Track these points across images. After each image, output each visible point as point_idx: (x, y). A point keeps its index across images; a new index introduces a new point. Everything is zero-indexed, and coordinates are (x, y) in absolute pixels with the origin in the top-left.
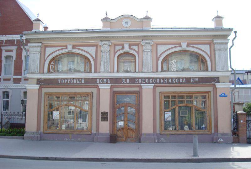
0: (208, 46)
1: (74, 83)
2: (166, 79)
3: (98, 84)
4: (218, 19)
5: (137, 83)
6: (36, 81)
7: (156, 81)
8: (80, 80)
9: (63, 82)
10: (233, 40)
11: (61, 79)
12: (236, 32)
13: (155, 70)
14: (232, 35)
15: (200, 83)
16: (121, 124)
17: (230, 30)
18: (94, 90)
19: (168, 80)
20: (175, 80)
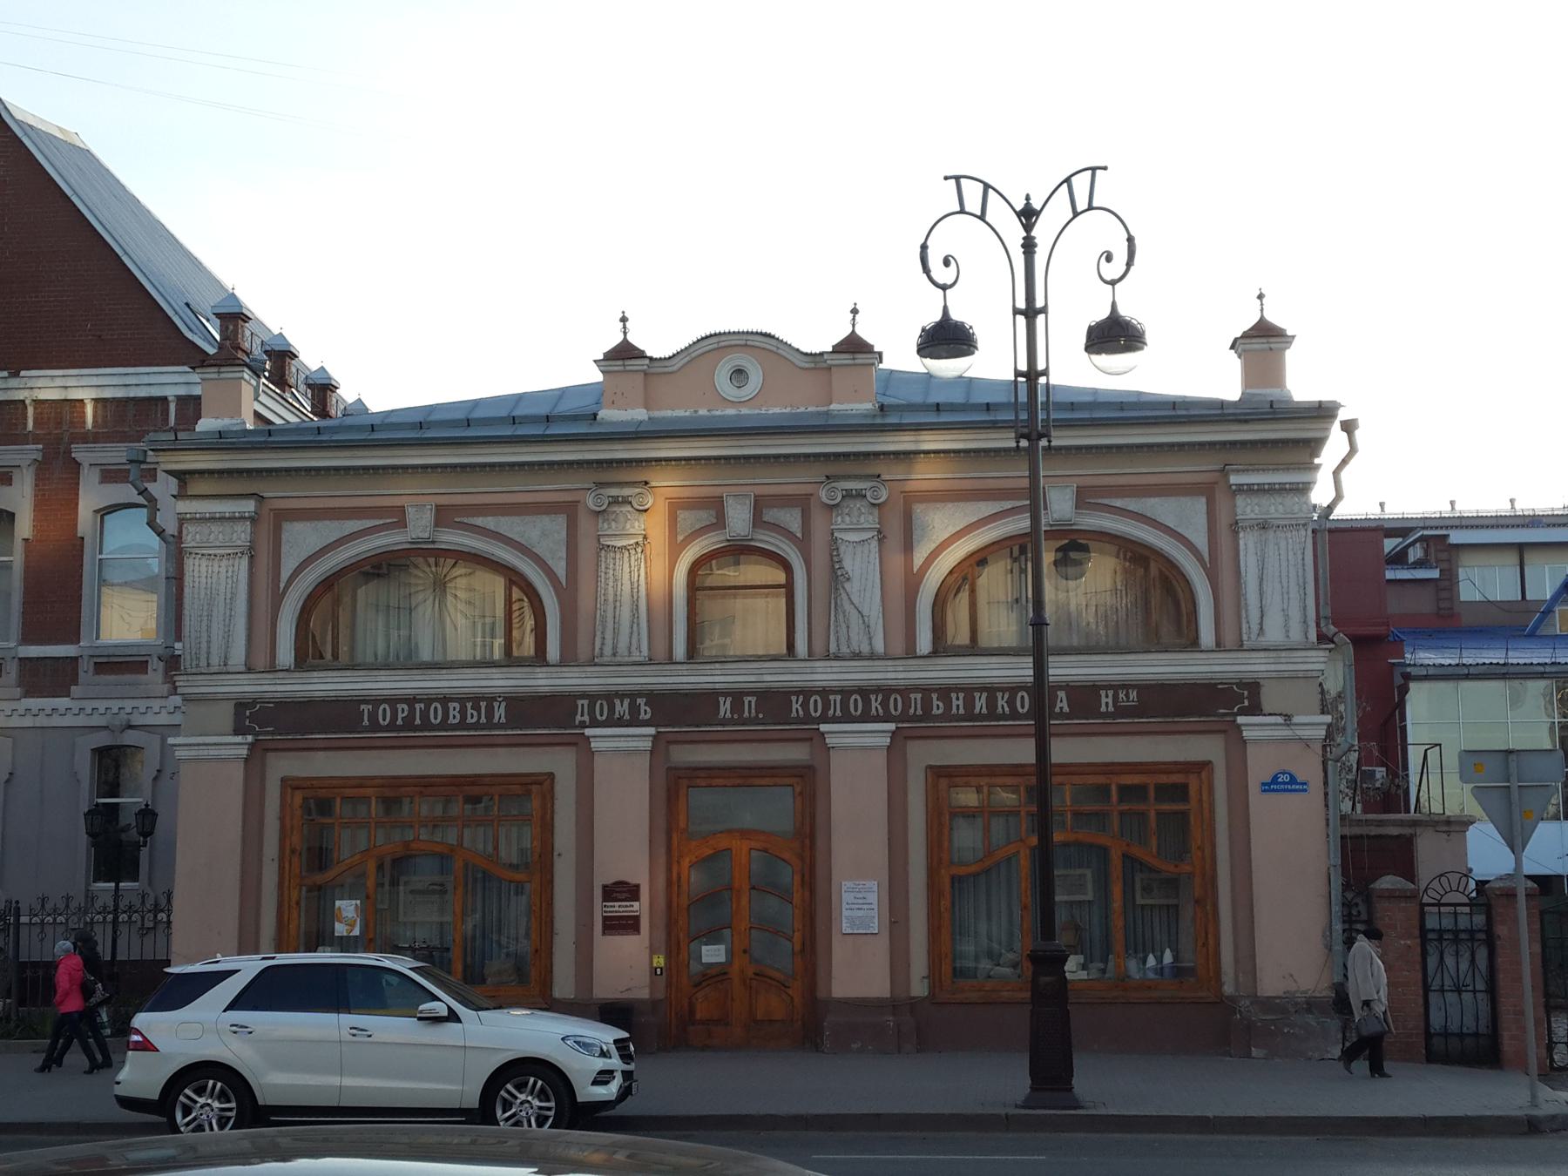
0: (1200, 504)
1: (451, 720)
2: (961, 695)
3: (583, 725)
4: (1262, 343)
5: (798, 721)
6: (226, 712)
7: (906, 705)
8: (483, 704)
9: (384, 715)
10: (1336, 473)
11: (376, 702)
12: (1349, 427)
13: (898, 647)
14: (1335, 445)
15: (1184, 716)
16: (713, 954)
17: (1323, 412)
18: (560, 763)
19: (969, 703)
20: (1011, 702)
